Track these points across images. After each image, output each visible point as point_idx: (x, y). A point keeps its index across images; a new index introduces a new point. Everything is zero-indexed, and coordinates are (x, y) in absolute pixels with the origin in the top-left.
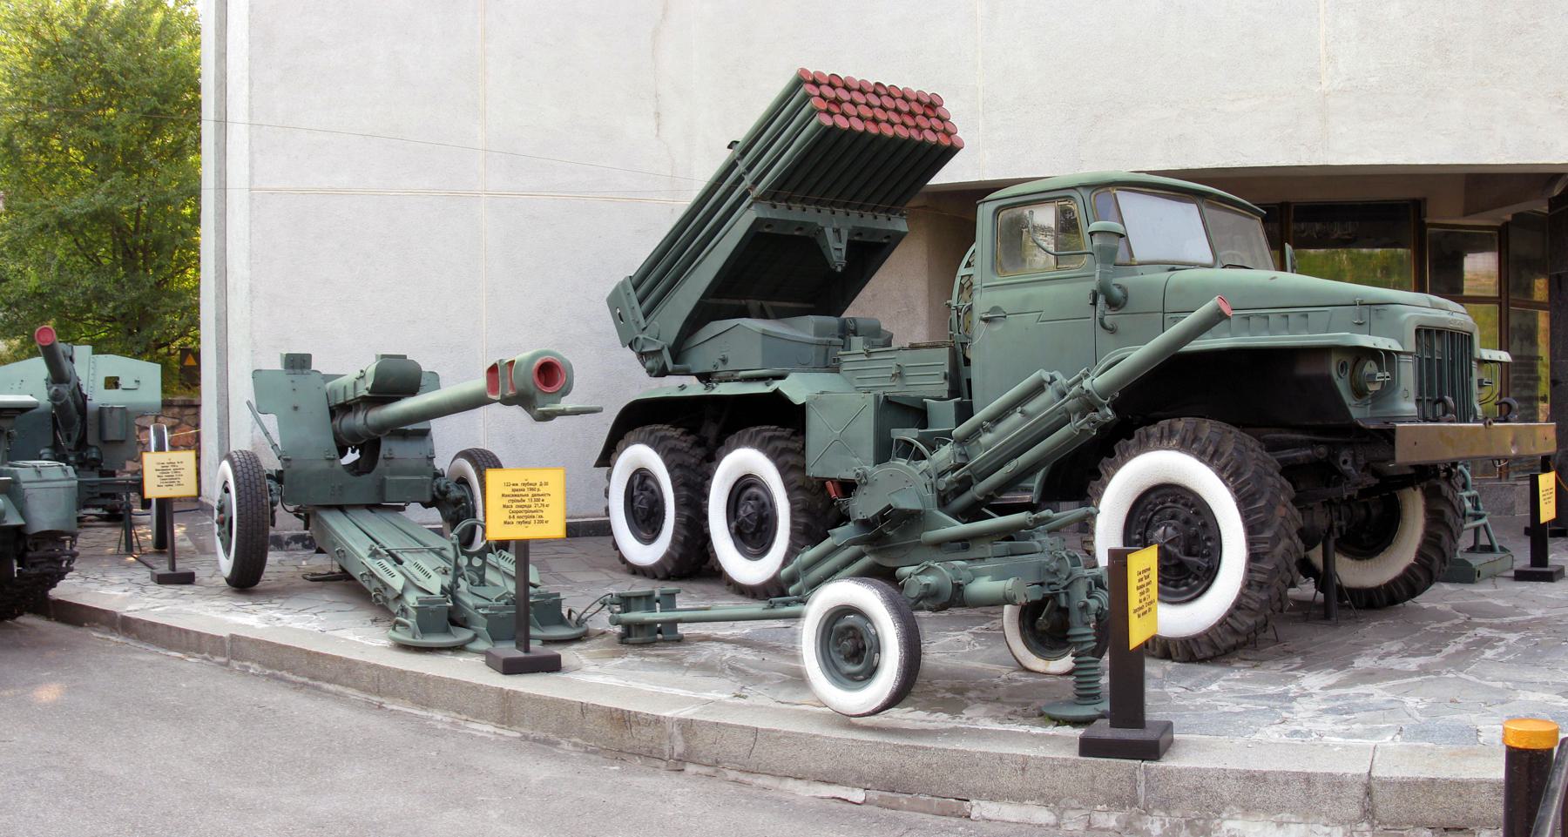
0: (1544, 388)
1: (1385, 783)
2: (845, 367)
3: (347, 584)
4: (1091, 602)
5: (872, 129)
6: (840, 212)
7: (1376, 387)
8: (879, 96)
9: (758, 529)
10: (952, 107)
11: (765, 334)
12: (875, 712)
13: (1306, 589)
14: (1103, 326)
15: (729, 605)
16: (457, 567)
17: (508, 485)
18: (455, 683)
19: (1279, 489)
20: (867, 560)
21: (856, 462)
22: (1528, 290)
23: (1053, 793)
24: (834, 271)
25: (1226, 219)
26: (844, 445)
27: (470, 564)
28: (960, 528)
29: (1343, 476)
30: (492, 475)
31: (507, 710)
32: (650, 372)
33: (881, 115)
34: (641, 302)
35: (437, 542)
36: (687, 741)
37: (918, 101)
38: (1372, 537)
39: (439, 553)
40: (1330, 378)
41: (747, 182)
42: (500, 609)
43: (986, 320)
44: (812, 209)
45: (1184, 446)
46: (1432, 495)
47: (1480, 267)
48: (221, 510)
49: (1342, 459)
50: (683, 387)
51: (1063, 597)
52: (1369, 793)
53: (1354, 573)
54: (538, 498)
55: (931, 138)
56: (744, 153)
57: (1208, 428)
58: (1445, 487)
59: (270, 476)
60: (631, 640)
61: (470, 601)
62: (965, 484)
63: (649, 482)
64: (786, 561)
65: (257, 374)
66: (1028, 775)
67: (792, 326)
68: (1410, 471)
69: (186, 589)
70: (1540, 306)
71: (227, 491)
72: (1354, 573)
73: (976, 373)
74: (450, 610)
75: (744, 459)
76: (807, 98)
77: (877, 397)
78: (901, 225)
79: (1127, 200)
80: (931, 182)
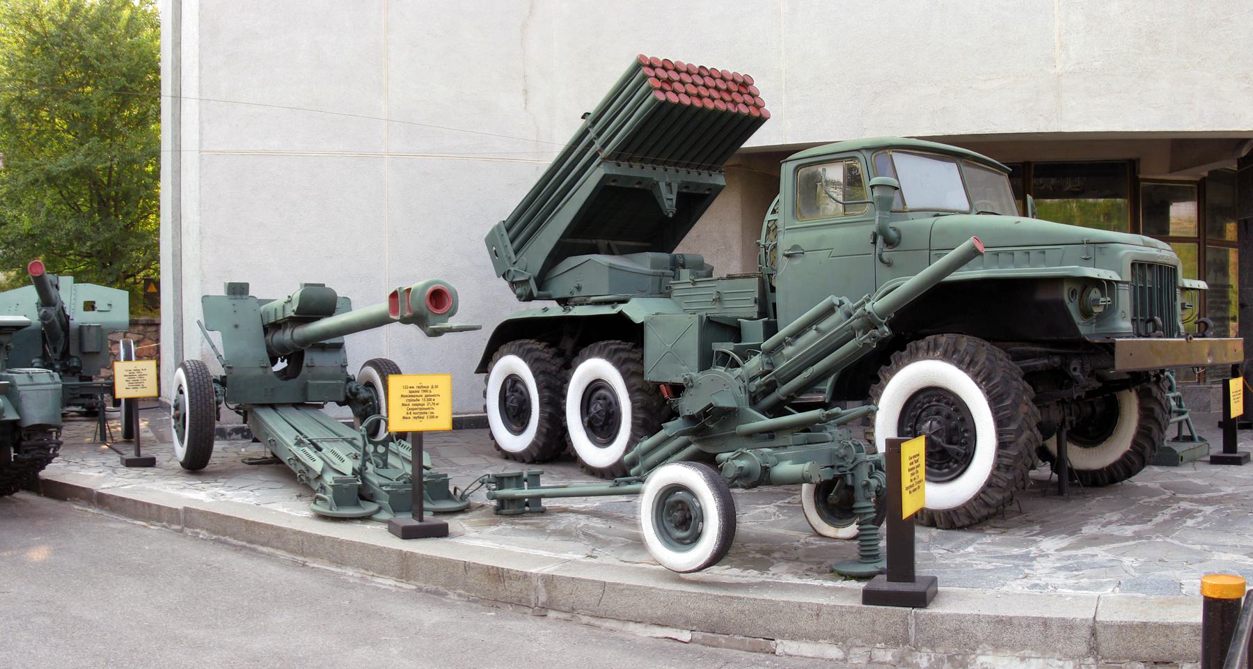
0: (1234, 310)
1: (1107, 626)
2: (675, 293)
3: (277, 467)
4: (872, 481)
5: (697, 103)
6: (672, 170)
7: (1100, 310)
8: (702, 76)
9: (606, 423)
10: (761, 86)
11: (611, 267)
12: (699, 569)
13: (1044, 471)
14: (882, 260)
15: (582, 484)
16: (365, 453)
17: (406, 387)
18: (363, 546)
19: (1022, 391)
20: (693, 448)
21: (684, 369)
22: (1221, 231)
23: (841, 634)
24: (667, 217)
25: (980, 175)
26: (674, 355)
27: (375, 451)
28: (767, 422)
29: (1073, 381)
30: (393, 380)
31: (405, 567)
32: (520, 297)
33: (704, 92)
34: (512, 242)
35: (349, 433)
36: (549, 592)
37: (733, 80)
38: (1097, 429)
39: (351, 442)
40: (1062, 302)
41: (597, 146)
42: (400, 487)
43: (788, 256)
44: (649, 167)
45: (947, 357)
46: (1145, 396)
47: (1183, 213)
48: (177, 408)
49: (1072, 367)
50: (545, 310)
51: (849, 477)
52: (1094, 633)
53: (1082, 458)
54: (430, 398)
55: (744, 110)
56: (594, 123)
57: (965, 342)
58: (1154, 389)
59: (215, 381)
60: (504, 511)
61: (376, 480)
62: (771, 387)
63: (519, 385)
64: (628, 448)
65: (205, 299)
66: (821, 620)
67: (633, 261)
68: (1127, 377)
69: (149, 471)
70: (1231, 244)
71: (181, 392)
72: (1082, 458)
73: (780, 298)
74: (359, 488)
75: (594, 367)
76: (645, 78)
77: (701, 318)
78: (720, 180)
79: (900, 160)
80: (744, 146)
